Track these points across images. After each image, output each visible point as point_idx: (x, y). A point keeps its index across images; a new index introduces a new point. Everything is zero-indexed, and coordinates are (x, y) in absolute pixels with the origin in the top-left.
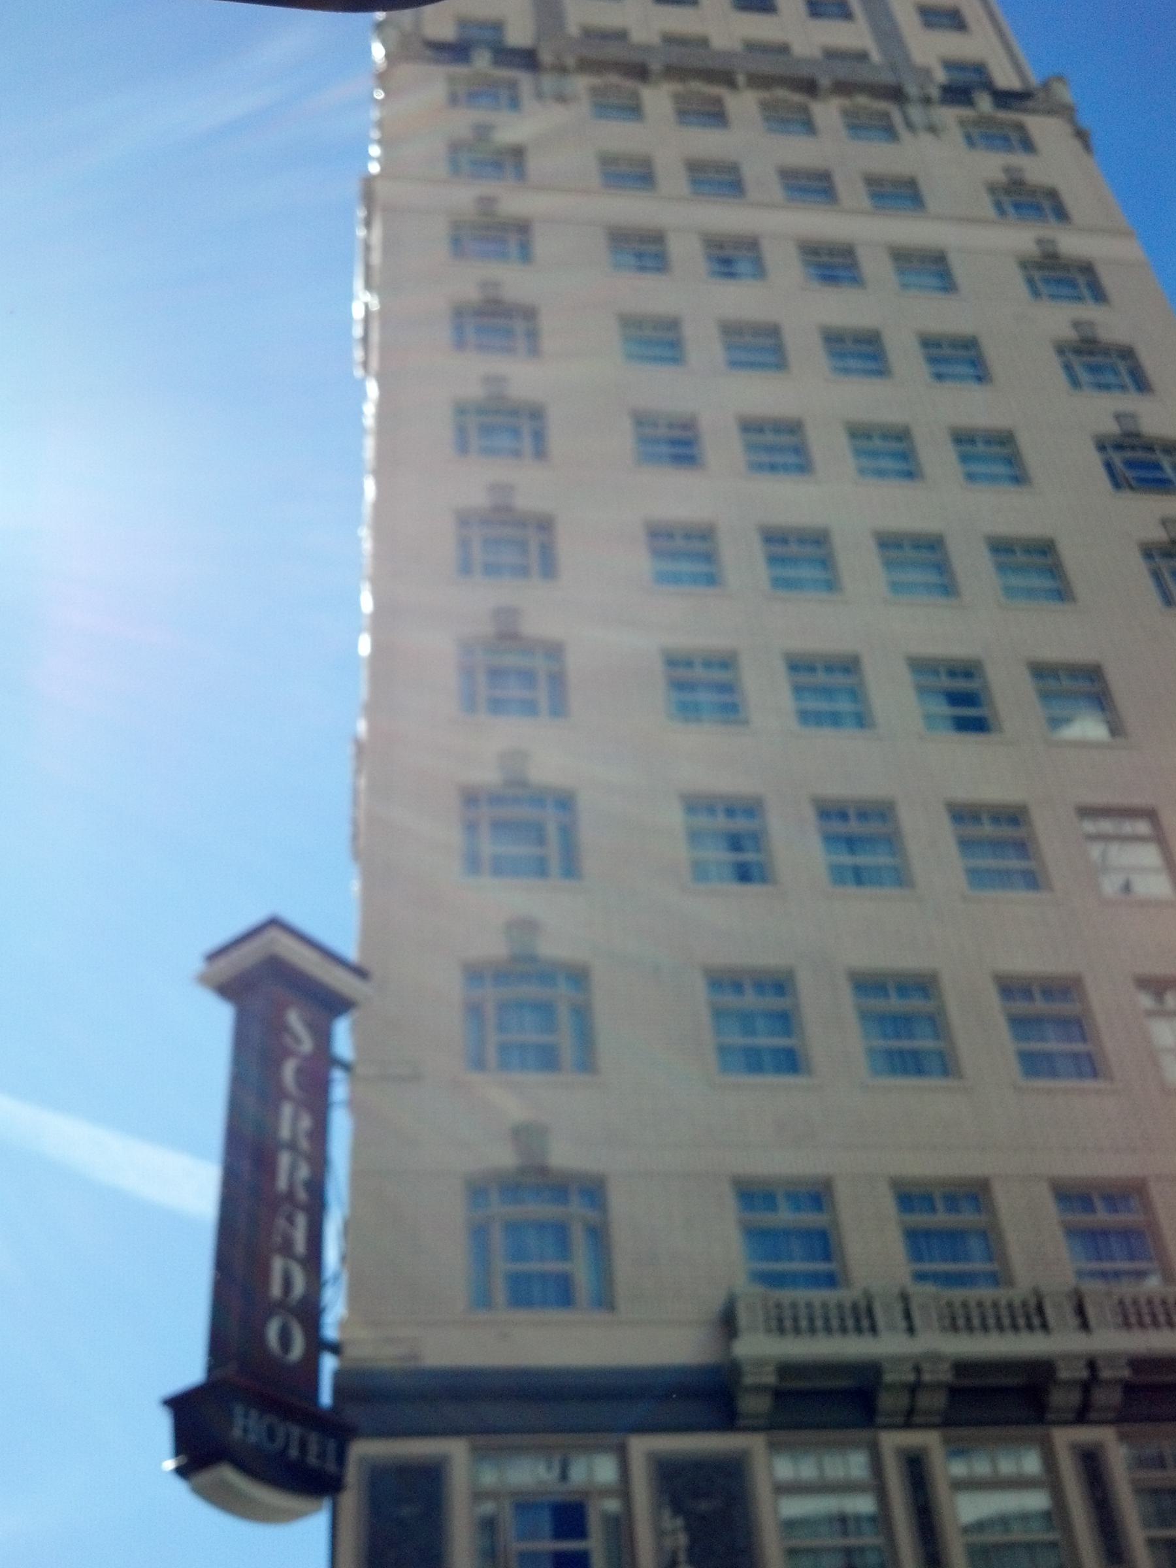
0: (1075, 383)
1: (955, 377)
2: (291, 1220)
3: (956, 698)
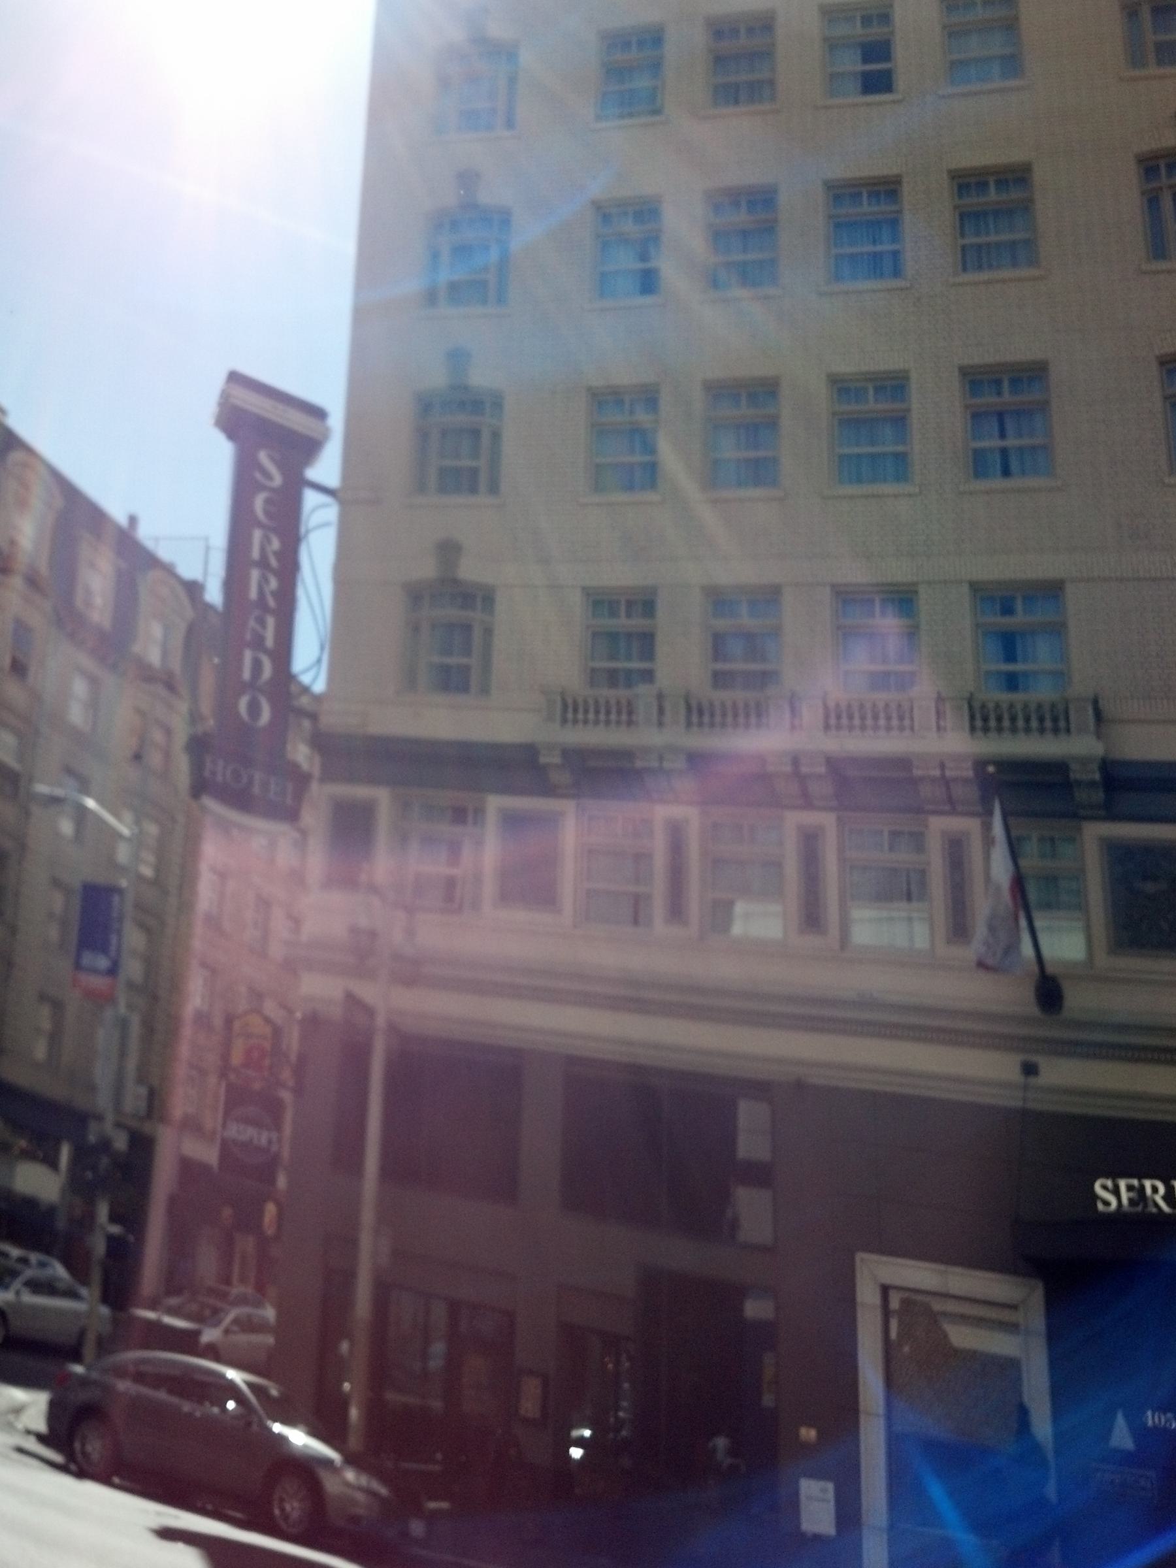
2: (262, 622)
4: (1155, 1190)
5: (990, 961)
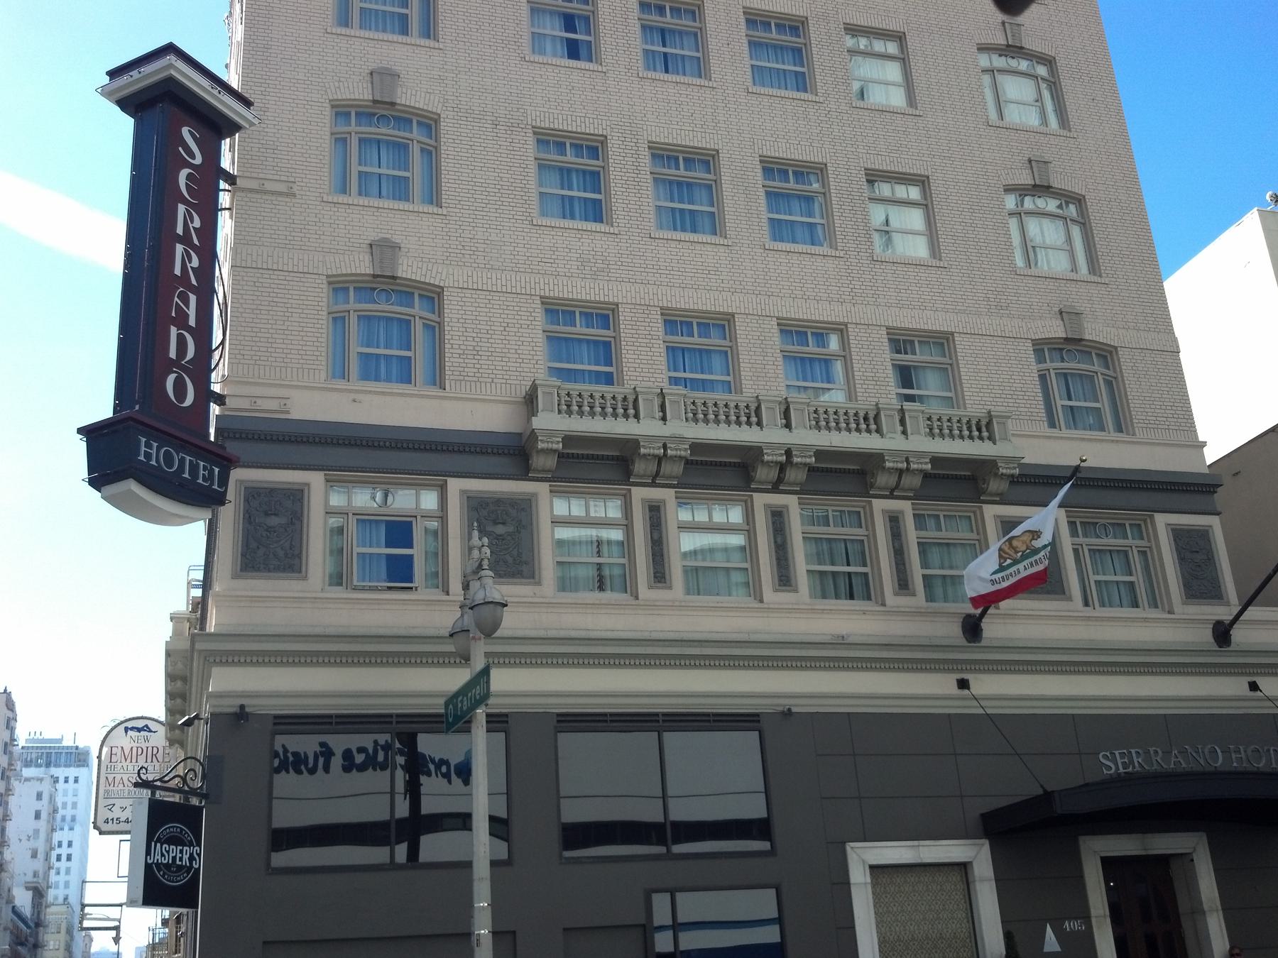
4: (1156, 752)
5: (499, 608)
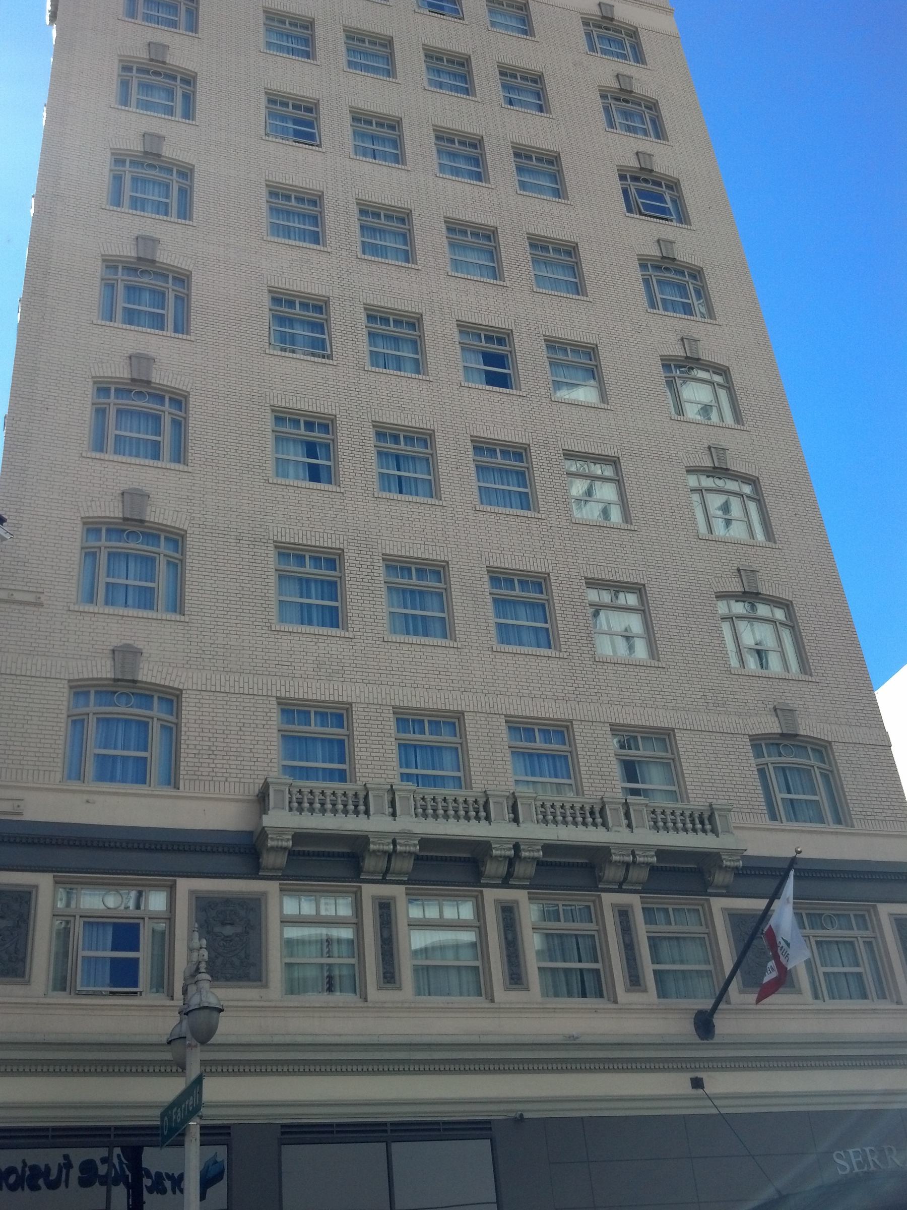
0: (611, 124)
1: (522, 103)
3: (490, 359)
